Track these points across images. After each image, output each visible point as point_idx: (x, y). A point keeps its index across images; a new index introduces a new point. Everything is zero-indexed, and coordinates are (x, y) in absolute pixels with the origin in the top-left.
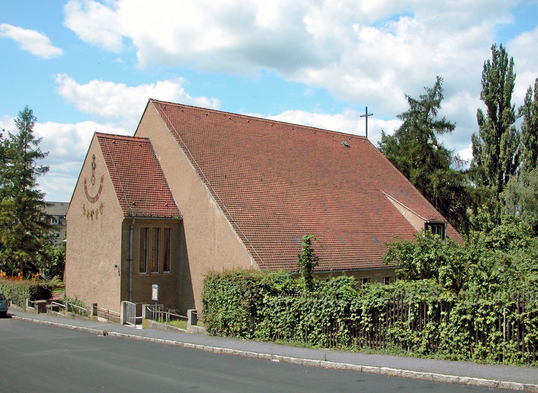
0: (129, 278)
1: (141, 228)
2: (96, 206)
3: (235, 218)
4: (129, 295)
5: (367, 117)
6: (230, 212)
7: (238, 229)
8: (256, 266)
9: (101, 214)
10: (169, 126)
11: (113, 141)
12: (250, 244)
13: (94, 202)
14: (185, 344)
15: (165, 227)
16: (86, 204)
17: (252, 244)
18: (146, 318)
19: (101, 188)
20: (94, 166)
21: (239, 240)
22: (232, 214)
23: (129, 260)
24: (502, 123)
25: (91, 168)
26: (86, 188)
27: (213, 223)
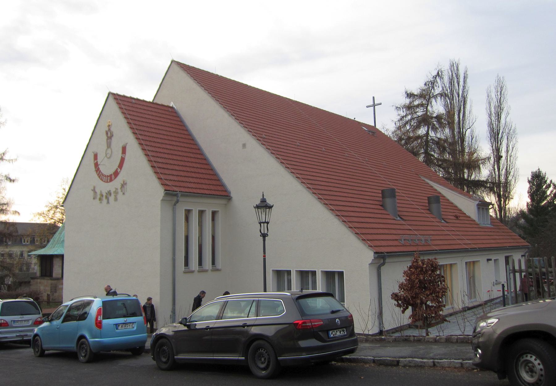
9: (124, 194)
15: (495, 259)
19: (122, 160)
20: (109, 135)
24: (473, 154)
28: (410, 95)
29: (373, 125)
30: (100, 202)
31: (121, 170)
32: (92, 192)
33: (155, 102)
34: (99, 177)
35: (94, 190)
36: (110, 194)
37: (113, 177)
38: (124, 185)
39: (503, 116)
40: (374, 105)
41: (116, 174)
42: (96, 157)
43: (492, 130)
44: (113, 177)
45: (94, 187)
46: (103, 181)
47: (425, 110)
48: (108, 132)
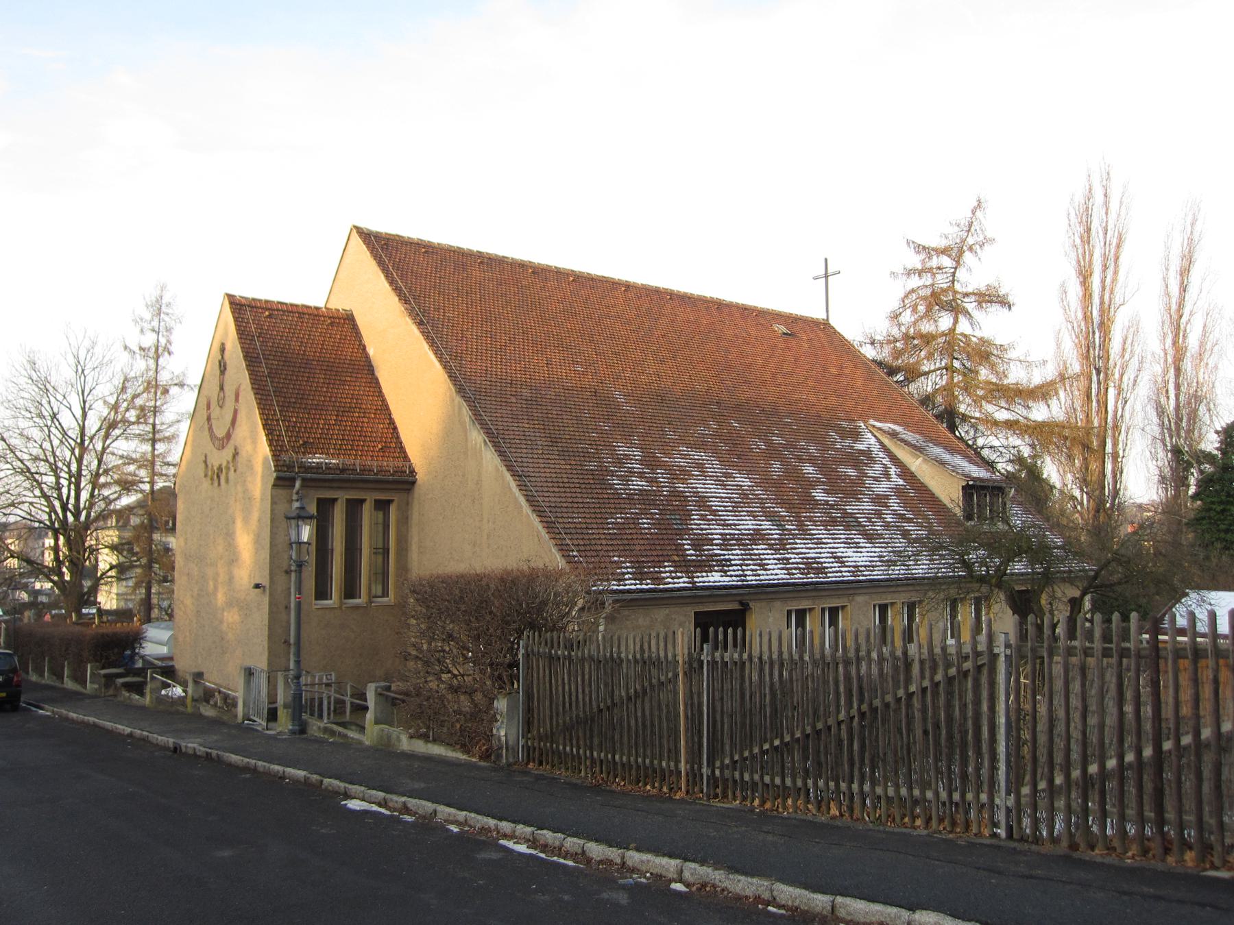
2: (227, 453)
3: (526, 469)
4: (289, 653)
5: (826, 277)
6: (515, 455)
7: (530, 493)
8: (561, 563)
9: (235, 471)
10: (391, 282)
11: (267, 313)
12: (558, 525)
13: (223, 448)
16: (209, 455)
17: (562, 526)
18: (377, 722)
19: (236, 412)
21: (535, 519)
22: (519, 460)
25: (218, 372)
26: (209, 419)
27: (477, 484)
28: (920, 249)
29: (820, 315)
32: (204, 464)
38: (236, 454)
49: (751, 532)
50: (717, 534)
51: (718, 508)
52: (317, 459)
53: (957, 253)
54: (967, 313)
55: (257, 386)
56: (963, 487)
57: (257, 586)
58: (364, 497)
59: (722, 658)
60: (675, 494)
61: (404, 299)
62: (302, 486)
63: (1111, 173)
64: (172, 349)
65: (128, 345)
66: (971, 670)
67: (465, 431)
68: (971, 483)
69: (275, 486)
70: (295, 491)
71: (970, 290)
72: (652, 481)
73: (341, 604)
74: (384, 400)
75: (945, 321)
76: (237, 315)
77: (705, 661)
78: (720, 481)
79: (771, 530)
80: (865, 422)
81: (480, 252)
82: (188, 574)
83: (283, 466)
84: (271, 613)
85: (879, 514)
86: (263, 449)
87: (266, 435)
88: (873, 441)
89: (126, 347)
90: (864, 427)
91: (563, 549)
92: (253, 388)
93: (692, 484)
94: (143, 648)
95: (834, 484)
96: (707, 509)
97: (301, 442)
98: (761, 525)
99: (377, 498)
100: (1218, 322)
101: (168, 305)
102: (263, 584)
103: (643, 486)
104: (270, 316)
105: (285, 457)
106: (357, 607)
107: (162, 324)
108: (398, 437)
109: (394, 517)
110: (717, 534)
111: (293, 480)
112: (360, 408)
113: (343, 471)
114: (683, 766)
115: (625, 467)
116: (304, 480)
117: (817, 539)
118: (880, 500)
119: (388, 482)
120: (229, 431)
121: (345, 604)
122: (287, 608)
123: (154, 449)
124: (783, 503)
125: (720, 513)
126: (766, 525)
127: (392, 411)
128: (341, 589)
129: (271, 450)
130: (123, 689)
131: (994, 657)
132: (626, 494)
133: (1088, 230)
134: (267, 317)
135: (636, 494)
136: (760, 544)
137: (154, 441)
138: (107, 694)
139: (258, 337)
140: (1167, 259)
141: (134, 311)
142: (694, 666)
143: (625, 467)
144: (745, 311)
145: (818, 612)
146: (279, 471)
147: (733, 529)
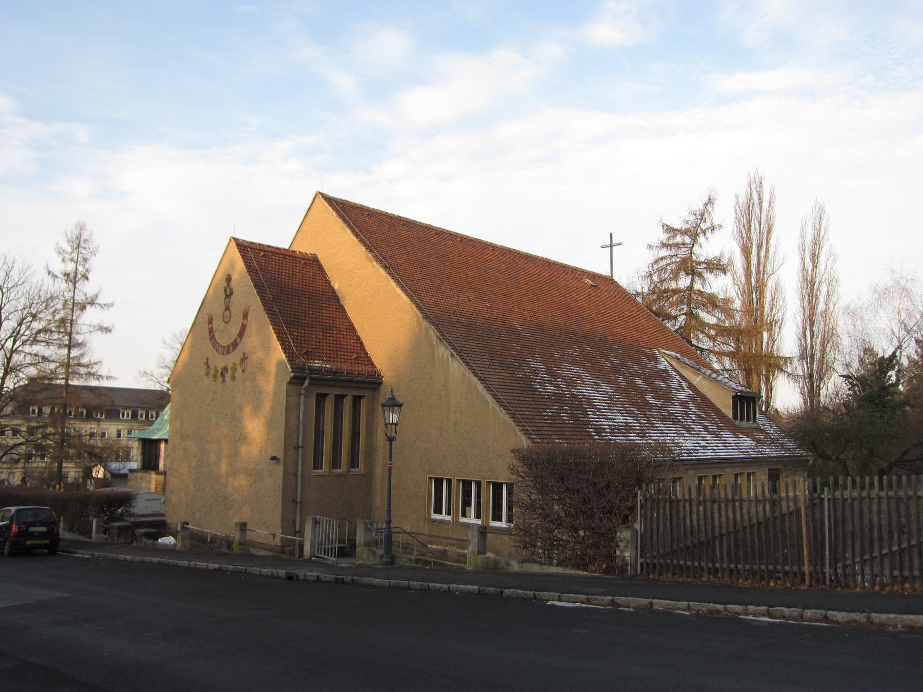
0: (297, 480)
1: (317, 394)
2: (234, 358)
9: (243, 371)
14: (507, 592)
16: (211, 358)
19: (243, 328)
20: (228, 293)
23: (297, 448)
28: (669, 229)
29: (607, 273)
30: (214, 379)
31: (241, 339)
32: (205, 366)
33: (292, 249)
34: (214, 347)
35: (207, 364)
36: (227, 371)
37: (231, 348)
38: (244, 358)
39: (822, 259)
40: (611, 246)
41: (235, 345)
42: (210, 321)
43: (805, 279)
44: (231, 348)
45: (207, 359)
46: (218, 352)
47: (690, 251)
48: (227, 288)
49: (623, 424)
50: (606, 425)
51: (601, 407)
52: (317, 364)
53: (693, 233)
54: (700, 275)
55: (267, 308)
56: (732, 396)
57: (274, 458)
58: (328, 392)
59: (842, 496)
60: (573, 396)
61: (369, 249)
62: (310, 384)
63: (763, 183)
64: (90, 276)
65: (51, 270)
66: (779, 517)
67: (432, 347)
68: (739, 394)
69: (290, 383)
70: (303, 387)
71: (702, 259)
72: (557, 386)
73: (330, 472)
74: (350, 322)
75: (684, 282)
76: (243, 254)
77: (826, 499)
78: (594, 388)
79: (634, 423)
80: (658, 350)
81: (400, 217)
82: (185, 449)
83: (297, 368)
84: (285, 478)
85: (687, 414)
86: (278, 353)
87: (281, 345)
88: (666, 363)
89: (49, 273)
90: (658, 353)
91: (526, 433)
92: (265, 309)
93: (580, 389)
94: (134, 507)
95: (657, 394)
96: (594, 407)
97: (304, 351)
98: (627, 420)
99: (355, 394)
100: (836, 289)
101: (86, 241)
102: (278, 456)
103: (553, 390)
104: (264, 256)
105: (297, 361)
106: (340, 475)
107: (80, 256)
108: (364, 350)
109: (365, 408)
110: (606, 425)
111: (304, 379)
112: (336, 327)
113: (335, 373)
114: (806, 568)
115: (539, 376)
116: (311, 379)
117: (661, 430)
118: (683, 404)
119: (364, 382)
120: (235, 340)
121: (333, 472)
122: (296, 475)
123: (69, 352)
124: (634, 405)
125: (603, 411)
126: (630, 420)
127: (358, 330)
128: (348, 460)
129: (286, 356)
130: (143, 537)
131: (799, 510)
132: (547, 395)
133: (749, 222)
134: (262, 256)
135: (552, 396)
136: (631, 433)
137: (70, 347)
138: (119, 542)
139: (260, 271)
140: (803, 245)
141: (57, 244)
142: (814, 504)
143: (539, 376)
144: (574, 270)
145: (746, 475)
146: (295, 372)
147: (613, 422)
